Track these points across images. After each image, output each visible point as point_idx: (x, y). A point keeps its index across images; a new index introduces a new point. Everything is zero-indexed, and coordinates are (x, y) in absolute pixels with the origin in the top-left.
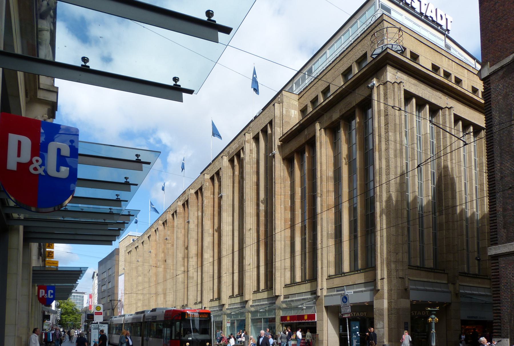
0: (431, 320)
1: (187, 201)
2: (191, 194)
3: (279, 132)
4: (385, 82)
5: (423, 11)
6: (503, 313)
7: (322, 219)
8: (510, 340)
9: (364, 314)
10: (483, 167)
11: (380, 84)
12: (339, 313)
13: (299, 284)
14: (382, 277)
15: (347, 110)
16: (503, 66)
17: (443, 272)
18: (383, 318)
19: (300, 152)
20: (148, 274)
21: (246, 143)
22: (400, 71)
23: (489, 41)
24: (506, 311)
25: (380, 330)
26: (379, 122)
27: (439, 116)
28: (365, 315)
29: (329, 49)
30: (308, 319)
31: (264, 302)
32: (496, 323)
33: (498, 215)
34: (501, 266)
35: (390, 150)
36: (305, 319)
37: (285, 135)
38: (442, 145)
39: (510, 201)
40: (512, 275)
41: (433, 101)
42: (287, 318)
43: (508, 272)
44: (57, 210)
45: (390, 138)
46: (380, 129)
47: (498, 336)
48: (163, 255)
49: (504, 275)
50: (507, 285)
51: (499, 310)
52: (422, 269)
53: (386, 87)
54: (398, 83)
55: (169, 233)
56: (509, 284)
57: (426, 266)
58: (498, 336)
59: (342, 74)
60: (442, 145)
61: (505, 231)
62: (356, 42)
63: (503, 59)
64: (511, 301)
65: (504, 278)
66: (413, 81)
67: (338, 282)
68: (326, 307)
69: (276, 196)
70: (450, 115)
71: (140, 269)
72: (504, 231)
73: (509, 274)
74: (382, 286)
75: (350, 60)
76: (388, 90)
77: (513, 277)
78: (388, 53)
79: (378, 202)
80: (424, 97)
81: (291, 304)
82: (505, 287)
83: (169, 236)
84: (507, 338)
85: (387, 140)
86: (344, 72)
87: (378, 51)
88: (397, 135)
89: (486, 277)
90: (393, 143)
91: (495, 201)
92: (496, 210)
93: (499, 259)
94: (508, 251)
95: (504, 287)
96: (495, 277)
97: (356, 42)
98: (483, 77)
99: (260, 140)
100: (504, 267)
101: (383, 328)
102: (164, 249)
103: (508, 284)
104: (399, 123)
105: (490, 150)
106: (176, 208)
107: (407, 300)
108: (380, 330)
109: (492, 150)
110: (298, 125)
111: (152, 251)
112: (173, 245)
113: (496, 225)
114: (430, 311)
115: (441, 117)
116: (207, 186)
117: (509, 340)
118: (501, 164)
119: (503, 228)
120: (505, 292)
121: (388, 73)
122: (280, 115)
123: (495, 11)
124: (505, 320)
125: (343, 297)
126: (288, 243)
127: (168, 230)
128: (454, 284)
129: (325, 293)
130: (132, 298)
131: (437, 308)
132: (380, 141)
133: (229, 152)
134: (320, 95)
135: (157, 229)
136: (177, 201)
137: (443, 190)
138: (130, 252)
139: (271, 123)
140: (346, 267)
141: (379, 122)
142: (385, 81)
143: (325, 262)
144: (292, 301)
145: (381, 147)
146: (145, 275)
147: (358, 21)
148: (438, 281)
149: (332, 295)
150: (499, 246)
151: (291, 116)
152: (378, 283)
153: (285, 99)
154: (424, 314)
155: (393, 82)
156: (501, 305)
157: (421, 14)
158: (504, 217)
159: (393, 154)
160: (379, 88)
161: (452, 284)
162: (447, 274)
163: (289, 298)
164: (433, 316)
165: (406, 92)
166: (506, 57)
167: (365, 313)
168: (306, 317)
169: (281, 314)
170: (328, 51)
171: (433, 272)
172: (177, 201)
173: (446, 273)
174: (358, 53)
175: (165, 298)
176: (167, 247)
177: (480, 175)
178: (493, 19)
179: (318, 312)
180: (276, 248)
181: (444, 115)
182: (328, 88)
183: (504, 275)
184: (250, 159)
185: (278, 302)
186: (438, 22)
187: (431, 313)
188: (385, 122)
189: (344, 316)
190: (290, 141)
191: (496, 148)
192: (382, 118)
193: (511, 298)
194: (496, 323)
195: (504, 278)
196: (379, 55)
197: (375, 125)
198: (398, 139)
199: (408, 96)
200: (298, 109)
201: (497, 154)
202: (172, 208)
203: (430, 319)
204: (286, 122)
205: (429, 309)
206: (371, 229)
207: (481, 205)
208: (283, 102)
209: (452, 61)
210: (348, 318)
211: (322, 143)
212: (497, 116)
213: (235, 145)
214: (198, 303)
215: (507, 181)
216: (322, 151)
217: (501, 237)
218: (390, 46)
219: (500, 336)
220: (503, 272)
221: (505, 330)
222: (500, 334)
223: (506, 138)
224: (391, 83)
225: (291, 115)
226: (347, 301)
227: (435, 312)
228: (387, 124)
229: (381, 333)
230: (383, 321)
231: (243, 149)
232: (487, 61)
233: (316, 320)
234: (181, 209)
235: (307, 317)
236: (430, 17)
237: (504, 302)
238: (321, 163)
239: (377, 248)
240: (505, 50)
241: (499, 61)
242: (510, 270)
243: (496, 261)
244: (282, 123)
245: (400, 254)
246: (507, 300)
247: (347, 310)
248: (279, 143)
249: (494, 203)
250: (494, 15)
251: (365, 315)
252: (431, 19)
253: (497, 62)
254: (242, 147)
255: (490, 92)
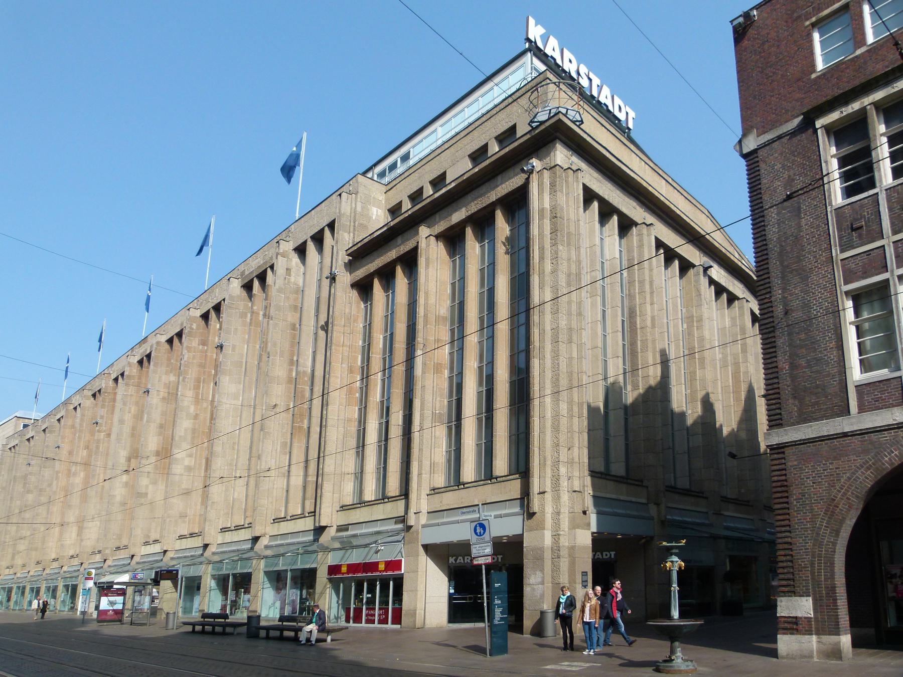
0: (670, 566)
1: (149, 356)
2: (158, 343)
3: (348, 239)
4: (552, 166)
5: (595, 93)
6: (796, 550)
7: (423, 387)
8: (812, 600)
9: (498, 558)
10: (693, 322)
11: (544, 168)
12: (450, 558)
13: (370, 504)
14: (541, 490)
15: (479, 208)
16: (781, 134)
17: (640, 483)
18: (543, 565)
19: (387, 275)
20: (48, 489)
21: (279, 257)
22: (576, 154)
23: (755, 98)
24: (802, 546)
25: (535, 587)
26: (540, 227)
27: (632, 235)
28: (500, 560)
29: (441, 126)
30: (348, 573)
31: (293, 538)
32: (783, 568)
33: (781, 375)
34: (790, 464)
35: (560, 273)
36: (380, 569)
37: (359, 245)
38: (637, 280)
39: (804, 351)
40: (812, 480)
41: (624, 210)
42: (380, 566)
43: (805, 476)
44: (263, 638)
45: (560, 254)
46: (543, 238)
47: (788, 592)
48: (85, 453)
49: (797, 480)
50: (802, 499)
51: (790, 543)
52: (608, 477)
53: (555, 173)
54: (574, 171)
55: (102, 412)
56: (806, 496)
57: (613, 473)
58: (788, 592)
59: (469, 156)
60: (637, 280)
61: (797, 402)
62: (497, 109)
63: (781, 125)
64: (813, 527)
65: (796, 485)
66: (596, 174)
67: (451, 499)
68: (426, 547)
69: (333, 347)
70: (649, 235)
71: (33, 479)
72: (793, 404)
73: (807, 478)
74: (543, 506)
75: (487, 135)
76: (558, 179)
77: (813, 483)
78: (560, 120)
79: (537, 358)
80: (611, 201)
81: (351, 542)
82: (799, 502)
83: (102, 417)
84: (807, 596)
85: (555, 258)
86: (474, 153)
87: (543, 117)
88: (572, 251)
89: (701, 495)
90: (565, 263)
91: (775, 352)
92: (776, 367)
93: (786, 452)
94: (804, 438)
95: (797, 502)
96: (779, 484)
97: (497, 109)
98: (746, 150)
99: (307, 252)
100: (796, 465)
101: (543, 583)
102: (89, 441)
103: (805, 496)
104: (574, 233)
105: (762, 268)
106: (124, 367)
107: (586, 531)
108: (535, 587)
109: (765, 266)
110: (385, 228)
111: (62, 445)
112: (109, 435)
113: (779, 393)
114: (668, 549)
115: (635, 238)
116: (193, 329)
117: (810, 599)
118: (784, 290)
119: (792, 398)
120: (799, 511)
121: (558, 153)
122: (351, 213)
123: (762, 54)
124: (802, 562)
125: (474, 524)
126: (353, 428)
127: (103, 406)
128: (658, 504)
129: (423, 520)
130: (6, 534)
131: (682, 542)
132: (542, 258)
133: (243, 273)
134: (428, 187)
135: (80, 405)
136: (127, 354)
137: (639, 351)
138: (14, 447)
139: (331, 226)
140: (469, 472)
141: (540, 227)
142: (553, 165)
143: (426, 464)
144: (355, 536)
145: (544, 267)
146: (41, 490)
147: (495, 88)
148: (634, 499)
149: (438, 525)
150: (785, 430)
151: (370, 218)
152: (533, 501)
153: (361, 189)
154: (607, 557)
155: (565, 168)
156: (792, 535)
157: (593, 97)
158: (793, 378)
159: (564, 280)
160: (542, 174)
161: (655, 504)
162: (647, 487)
163: (347, 530)
164: (675, 558)
165: (586, 189)
166: (786, 122)
167: (613, 553)
168: (382, 567)
169: (332, 559)
170: (440, 130)
171: (625, 483)
172: (127, 354)
173: (644, 486)
174: (501, 124)
175: (80, 534)
176: (96, 438)
177: (689, 334)
178: (760, 65)
179: (408, 556)
180: (327, 439)
181: (640, 235)
182: (442, 177)
183: (797, 480)
184: (285, 284)
185: (324, 538)
186: (615, 113)
187: (668, 551)
188: (551, 229)
189: (475, 562)
190: (367, 255)
191: (775, 264)
192: (547, 223)
193: (812, 521)
194: (783, 568)
195: (796, 485)
196: (542, 123)
197: (533, 232)
198: (574, 257)
199: (589, 196)
200: (384, 207)
201: (775, 273)
202: (115, 368)
203: (668, 565)
204: (361, 225)
205: (664, 543)
206: (518, 407)
207: (691, 381)
208: (358, 192)
209: (646, 163)
210: (486, 565)
211: (430, 260)
212: (773, 213)
213: (257, 261)
214: (151, 542)
215: (797, 318)
216: (430, 274)
217: (789, 413)
218: (564, 111)
219: (794, 592)
220: (794, 474)
221: (803, 580)
222: (792, 589)
223: (792, 248)
224: (562, 168)
225: (370, 214)
226: (484, 533)
227: (677, 551)
228: (554, 231)
229: (538, 593)
230: (542, 570)
231: (272, 267)
232: (752, 127)
233: (403, 572)
234: (135, 371)
235: (346, 568)
236: (605, 104)
237: (798, 529)
238: (426, 293)
239: (534, 438)
240: (784, 111)
241: (774, 128)
242: (809, 472)
243: (781, 456)
244: (354, 226)
245: (576, 450)
246: (804, 525)
247: (485, 549)
248: (347, 259)
249: (773, 355)
250: (762, 59)
251: (500, 560)
252: (605, 107)
253: (770, 130)
254: (270, 264)
255: (759, 175)
